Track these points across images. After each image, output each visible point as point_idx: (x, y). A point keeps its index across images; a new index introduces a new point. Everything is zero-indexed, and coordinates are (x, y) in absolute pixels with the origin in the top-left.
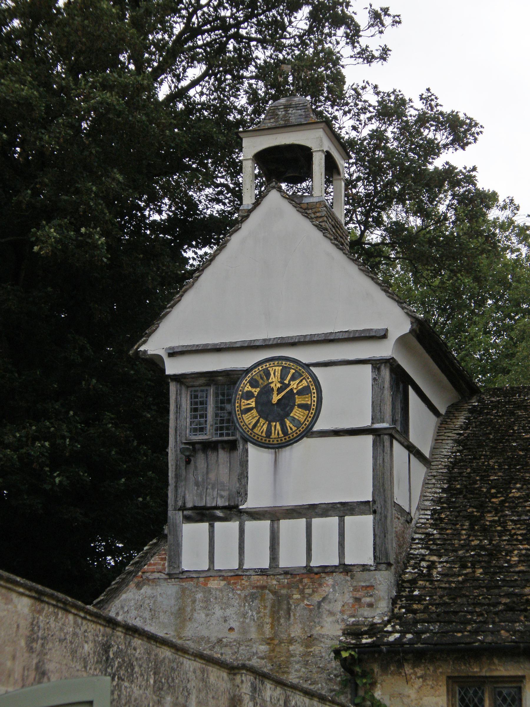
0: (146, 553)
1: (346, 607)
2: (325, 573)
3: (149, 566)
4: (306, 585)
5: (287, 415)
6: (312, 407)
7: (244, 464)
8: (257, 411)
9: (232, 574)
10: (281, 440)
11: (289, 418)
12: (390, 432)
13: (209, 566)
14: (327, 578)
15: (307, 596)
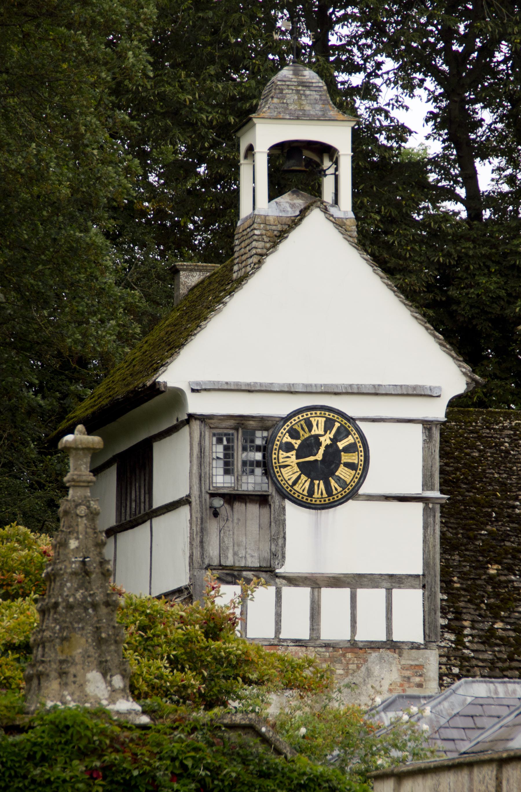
4: (350, 659)
5: (332, 473)
7: (282, 523)
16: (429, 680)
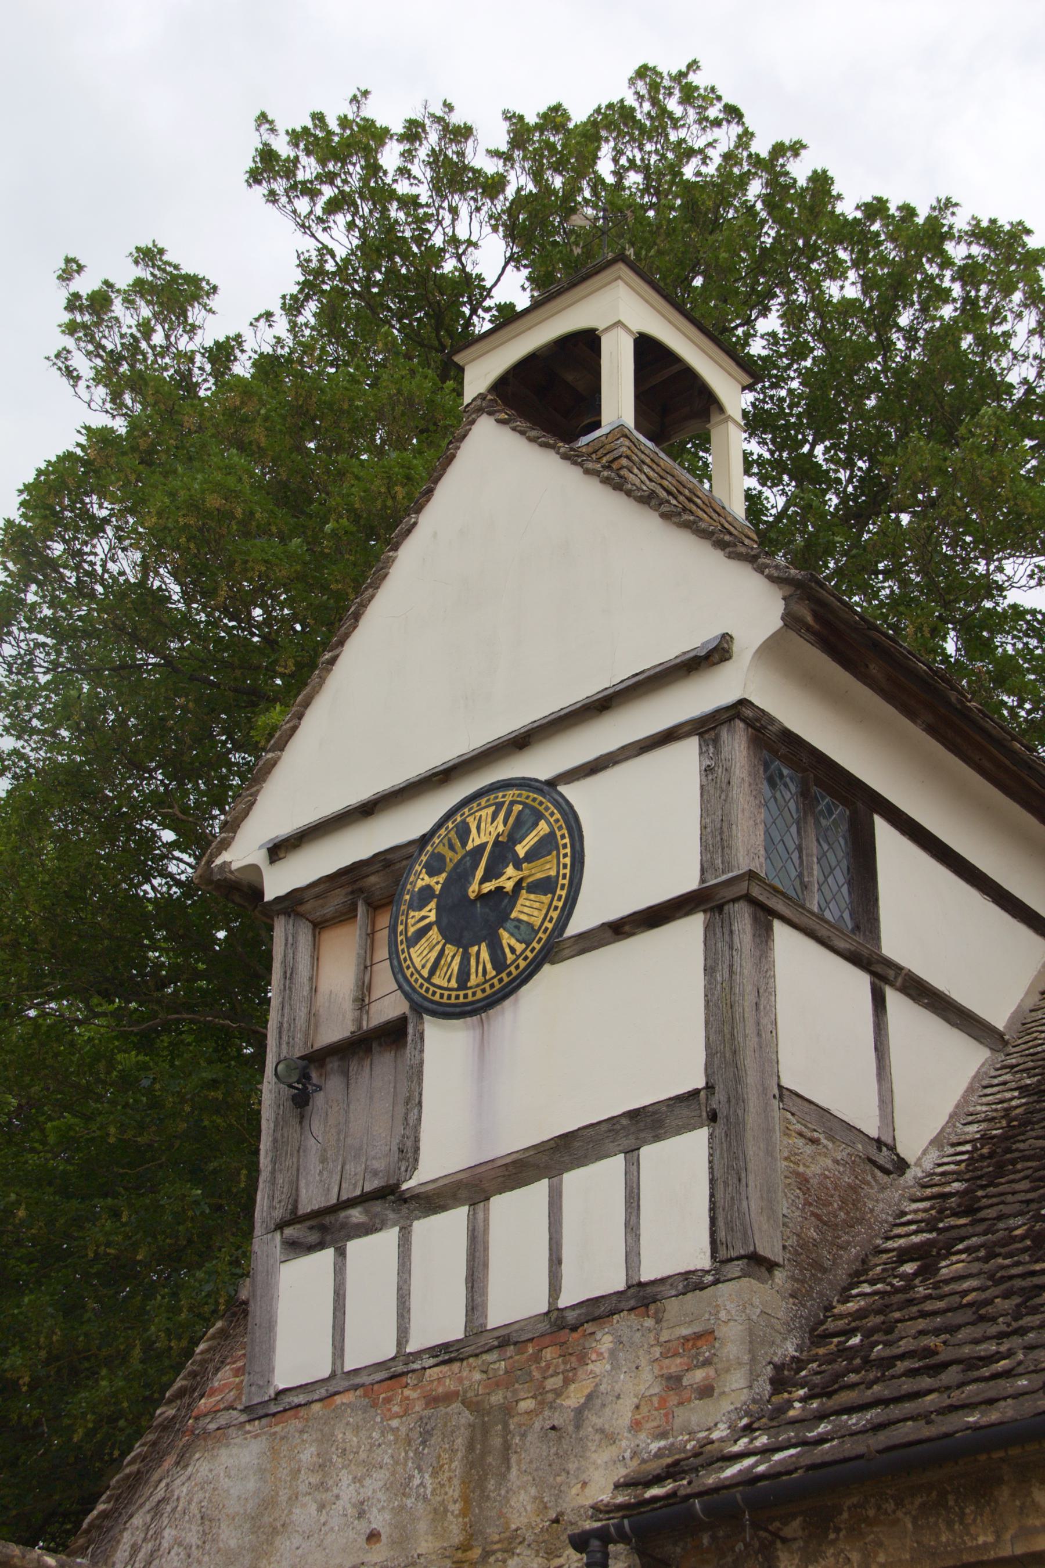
0: (203, 1363)
1: (644, 1410)
2: (594, 1320)
3: (210, 1396)
5: (503, 918)
6: (561, 881)
8: (439, 929)
9: (383, 1375)
10: (492, 986)
11: (509, 925)
12: (742, 888)
13: (334, 1364)
14: (598, 1336)
15: (550, 1397)
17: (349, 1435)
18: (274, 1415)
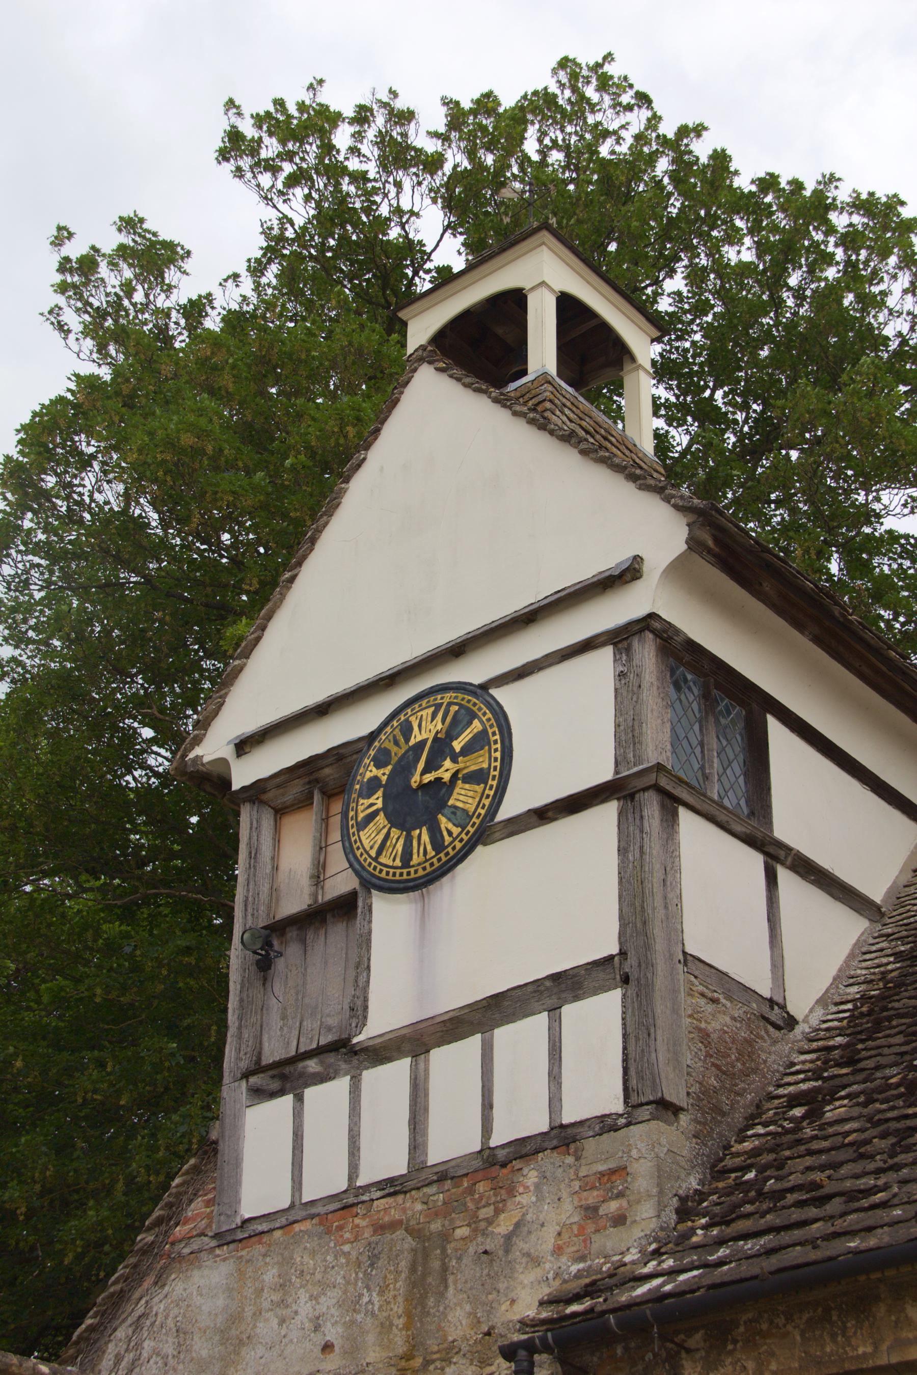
0: (178, 1195)
1: (565, 1236)
2: (521, 1157)
3: (184, 1224)
5: (442, 805)
6: (492, 773)
8: (385, 815)
9: (336, 1206)
10: (432, 865)
11: (447, 811)
13: (293, 1196)
14: (525, 1171)
15: (483, 1225)
16: (638, 1202)
17: (306, 1259)
18: (240, 1241)
